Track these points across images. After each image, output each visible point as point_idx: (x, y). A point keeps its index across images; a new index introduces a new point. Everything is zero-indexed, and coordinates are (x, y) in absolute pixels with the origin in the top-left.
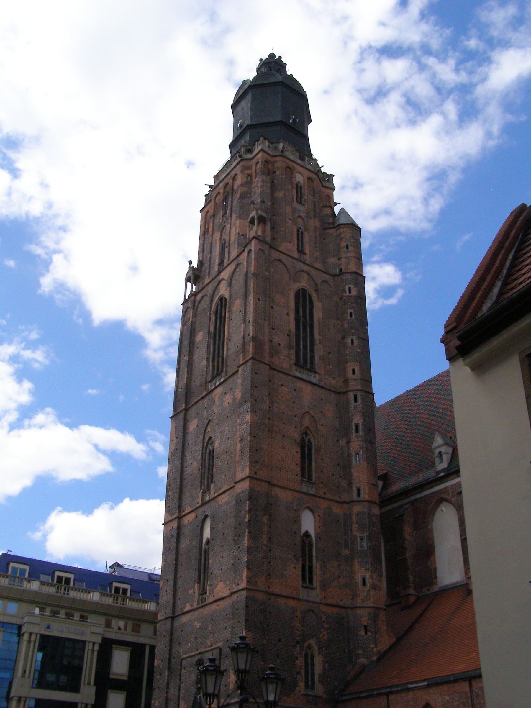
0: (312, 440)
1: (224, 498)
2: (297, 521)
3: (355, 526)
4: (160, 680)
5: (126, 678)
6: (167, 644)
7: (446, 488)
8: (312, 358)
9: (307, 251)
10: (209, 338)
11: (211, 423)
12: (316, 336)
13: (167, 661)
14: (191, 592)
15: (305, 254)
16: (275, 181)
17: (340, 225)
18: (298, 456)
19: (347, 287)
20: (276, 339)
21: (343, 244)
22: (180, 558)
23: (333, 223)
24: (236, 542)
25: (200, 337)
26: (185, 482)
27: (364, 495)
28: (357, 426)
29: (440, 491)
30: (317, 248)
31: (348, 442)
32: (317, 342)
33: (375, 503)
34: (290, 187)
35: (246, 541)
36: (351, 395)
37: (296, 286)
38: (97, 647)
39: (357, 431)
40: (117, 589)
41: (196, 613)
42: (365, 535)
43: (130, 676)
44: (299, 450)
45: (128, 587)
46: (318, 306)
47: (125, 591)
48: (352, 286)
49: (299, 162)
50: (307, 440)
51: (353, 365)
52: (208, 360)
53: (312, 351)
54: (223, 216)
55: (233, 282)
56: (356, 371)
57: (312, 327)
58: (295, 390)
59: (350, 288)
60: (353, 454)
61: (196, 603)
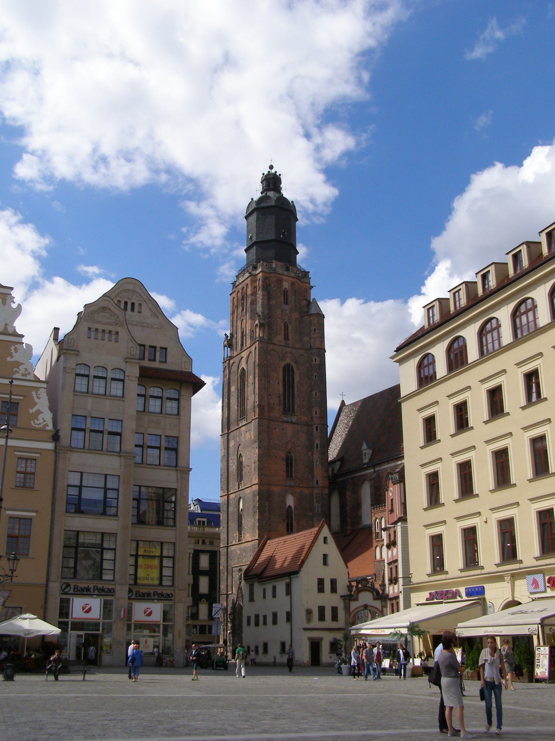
0: (293, 456)
1: (248, 490)
2: (284, 501)
3: (315, 500)
4: (223, 576)
5: (208, 569)
6: (226, 559)
7: (367, 474)
8: (293, 406)
9: (290, 338)
10: (238, 392)
11: (240, 446)
12: (296, 393)
13: (226, 567)
14: (235, 535)
15: (289, 340)
16: (270, 292)
17: (311, 314)
18: (284, 467)
19: (314, 358)
20: (272, 402)
21: (313, 328)
22: (229, 516)
23: (307, 312)
24: (253, 515)
25: (233, 389)
26: (230, 475)
27: (320, 484)
28: (317, 445)
29: (364, 475)
30: (297, 334)
31: (312, 454)
32: (296, 396)
33: (325, 487)
34: (279, 294)
35: (257, 516)
36: (315, 427)
37: (283, 364)
38: (191, 555)
39: (317, 448)
40: (199, 522)
41: (238, 546)
42: (319, 505)
43: (210, 568)
44: (285, 463)
45: (205, 520)
46: (296, 372)
47: (204, 522)
48: (317, 357)
49: (285, 273)
50: (290, 456)
51: (316, 409)
52: (238, 406)
53: (293, 401)
54: (242, 311)
55: (249, 362)
56: (317, 412)
57: (293, 387)
58: (283, 429)
59: (315, 359)
60: (315, 461)
61: (237, 541)
